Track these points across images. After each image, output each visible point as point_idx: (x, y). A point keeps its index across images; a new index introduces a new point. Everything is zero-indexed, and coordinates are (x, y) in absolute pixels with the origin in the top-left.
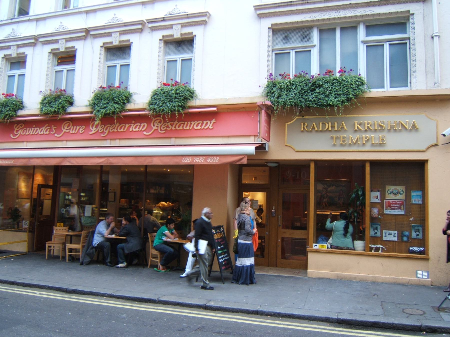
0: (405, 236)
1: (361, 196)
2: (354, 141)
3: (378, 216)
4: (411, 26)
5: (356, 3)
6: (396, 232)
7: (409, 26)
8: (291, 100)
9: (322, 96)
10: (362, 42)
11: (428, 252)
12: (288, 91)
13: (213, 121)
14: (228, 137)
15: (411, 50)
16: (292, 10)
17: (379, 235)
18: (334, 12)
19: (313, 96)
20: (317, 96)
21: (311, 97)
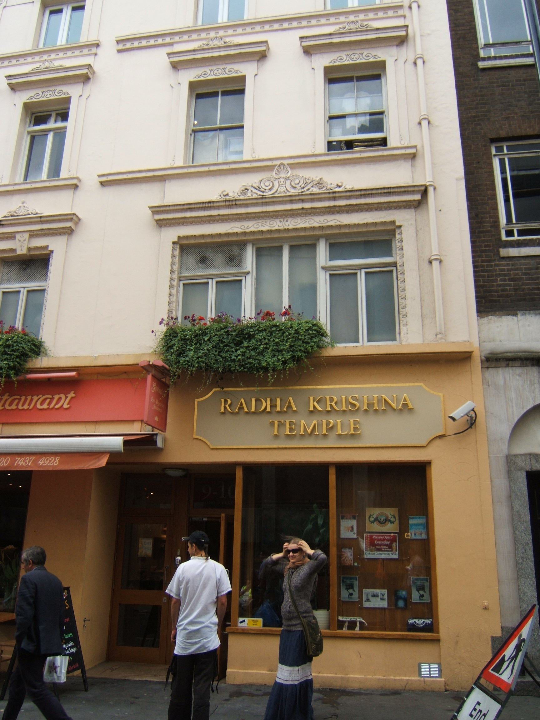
0: (401, 598)
1: (323, 526)
2: (309, 431)
3: (354, 563)
4: (398, 244)
5: (312, 208)
6: (385, 591)
7: (396, 244)
8: (200, 360)
9: (253, 353)
10: (323, 268)
11: (438, 628)
12: (198, 345)
13: (71, 395)
14: (96, 422)
15: (399, 282)
16: (211, 216)
17: (356, 597)
18: (278, 221)
19: (239, 352)
20: (245, 352)
21: (236, 354)
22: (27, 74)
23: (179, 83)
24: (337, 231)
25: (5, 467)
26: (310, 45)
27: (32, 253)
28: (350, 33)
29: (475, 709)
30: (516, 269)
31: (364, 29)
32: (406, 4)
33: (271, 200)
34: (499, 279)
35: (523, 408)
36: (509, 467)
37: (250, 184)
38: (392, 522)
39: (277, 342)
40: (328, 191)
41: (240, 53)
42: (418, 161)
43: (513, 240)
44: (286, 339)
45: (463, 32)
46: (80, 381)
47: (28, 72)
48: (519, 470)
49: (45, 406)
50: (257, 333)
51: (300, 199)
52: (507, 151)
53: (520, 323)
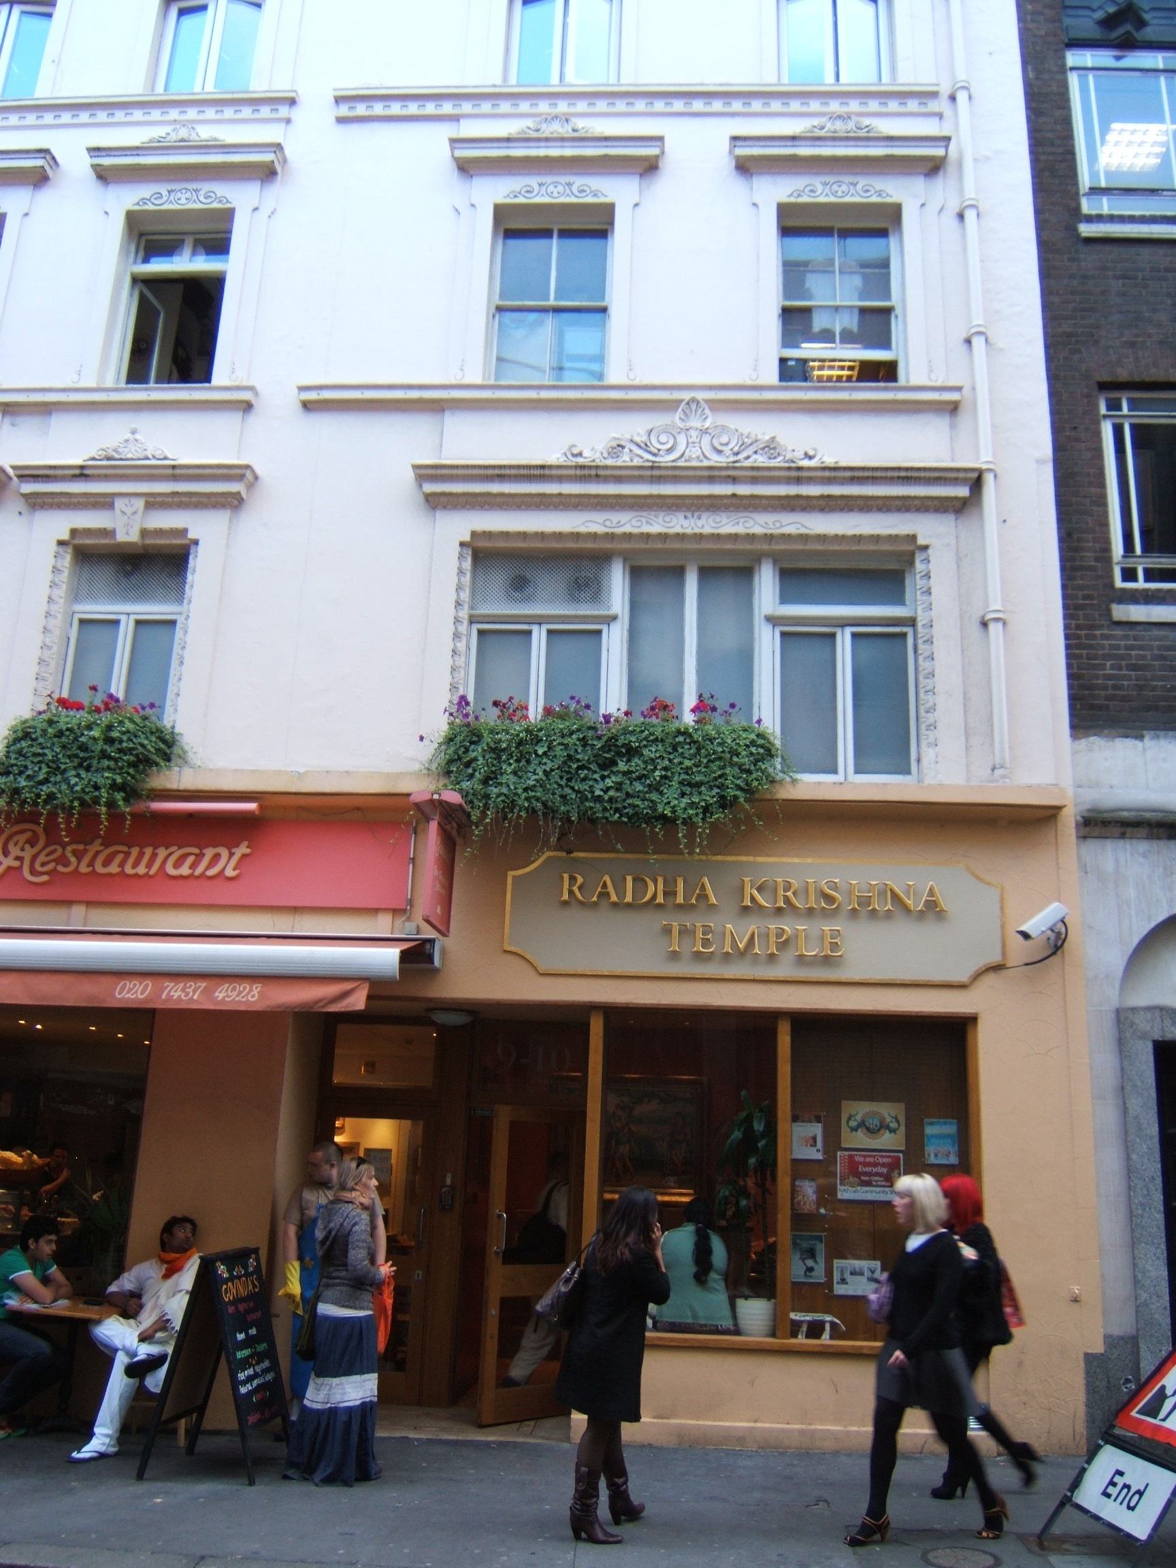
4: (920, 583)
8: (531, 794)
9: (638, 787)
10: (772, 620)
12: (523, 762)
13: (243, 849)
14: (296, 910)
15: (921, 658)
17: (819, 1275)
18: (681, 516)
19: (609, 782)
20: (620, 784)
22: (138, 148)
23: (473, 205)
24: (799, 547)
25: (142, 1001)
26: (752, 156)
27: (150, 541)
28: (834, 139)
29: (1112, 1483)
30: (1141, 648)
31: (862, 134)
32: (945, 90)
33: (670, 473)
34: (1108, 664)
35: (1149, 919)
36: (1120, 1032)
37: (628, 437)
38: (893, 1131)
39: (687, 768)
40: (787, 465)
41: (606, 156)
42: (964, 418)
43: (1136, 590)
44: (705, 761)
45: (1051, 158)
46: (262, 824)
47: (138, 144)
48: (1140, 1038)
49: (185, 870)
50: (645, 746)
51: (729, 476)
52: (1129, 410)
53: (1149, 754)
